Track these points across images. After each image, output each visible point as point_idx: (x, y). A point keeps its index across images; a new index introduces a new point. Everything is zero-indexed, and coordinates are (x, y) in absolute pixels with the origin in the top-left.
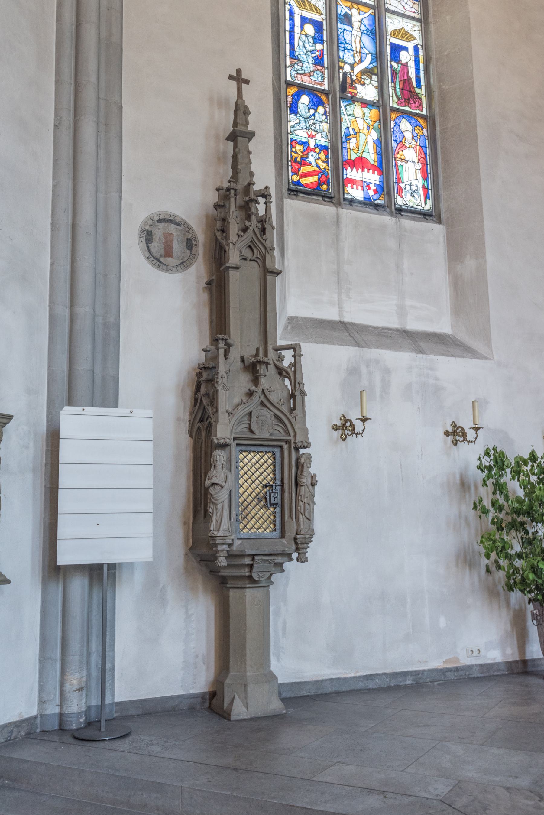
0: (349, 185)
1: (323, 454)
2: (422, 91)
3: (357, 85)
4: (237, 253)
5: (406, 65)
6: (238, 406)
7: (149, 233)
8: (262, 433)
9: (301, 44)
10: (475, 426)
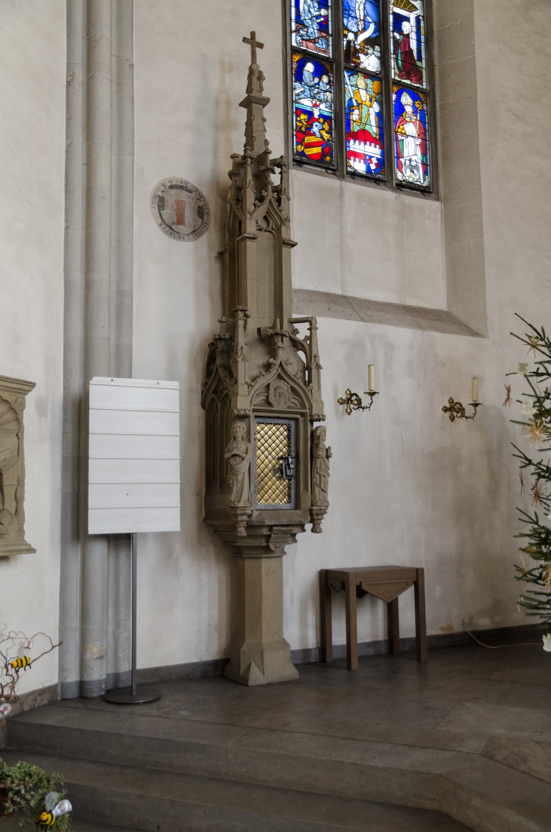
0: (352, 158)
1: (335, 429)
2: (423, 64)
3: (360, 55)
4: (254, 223)
5: (407, 36)
6: (256, 378)
7: (162, 199)
8: (279, 405)
9: (306, 8)
10: (473, 402)
